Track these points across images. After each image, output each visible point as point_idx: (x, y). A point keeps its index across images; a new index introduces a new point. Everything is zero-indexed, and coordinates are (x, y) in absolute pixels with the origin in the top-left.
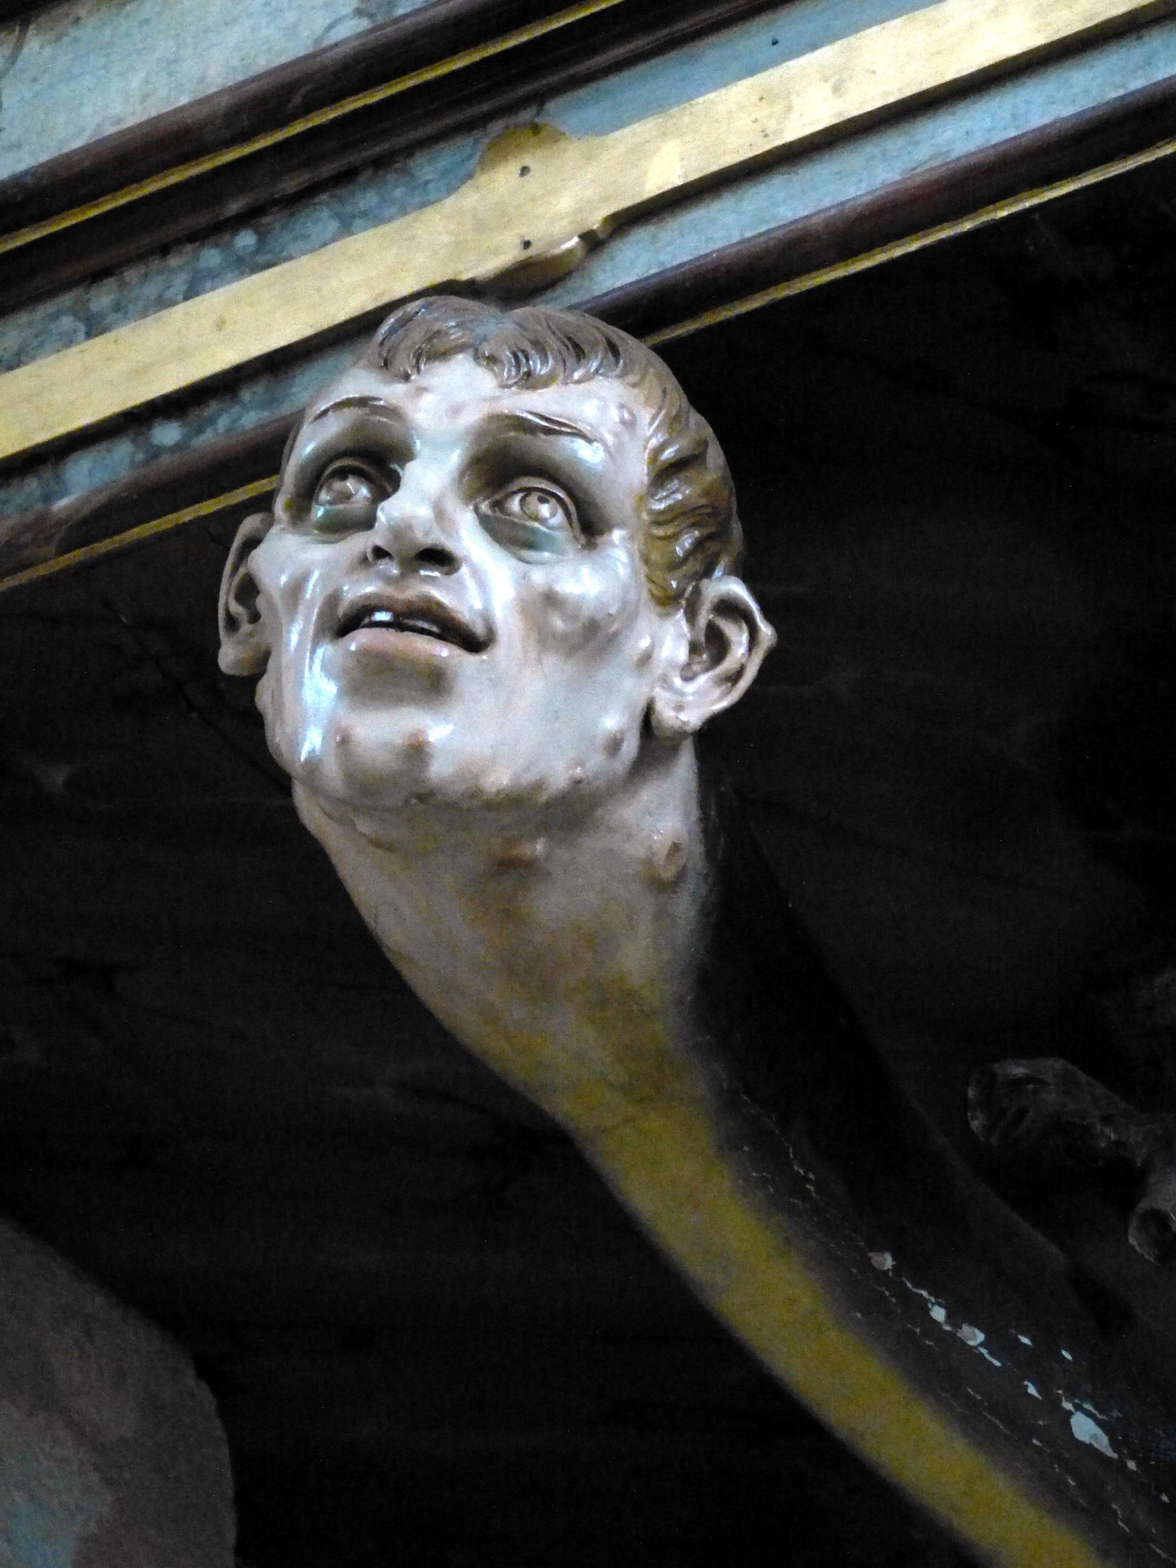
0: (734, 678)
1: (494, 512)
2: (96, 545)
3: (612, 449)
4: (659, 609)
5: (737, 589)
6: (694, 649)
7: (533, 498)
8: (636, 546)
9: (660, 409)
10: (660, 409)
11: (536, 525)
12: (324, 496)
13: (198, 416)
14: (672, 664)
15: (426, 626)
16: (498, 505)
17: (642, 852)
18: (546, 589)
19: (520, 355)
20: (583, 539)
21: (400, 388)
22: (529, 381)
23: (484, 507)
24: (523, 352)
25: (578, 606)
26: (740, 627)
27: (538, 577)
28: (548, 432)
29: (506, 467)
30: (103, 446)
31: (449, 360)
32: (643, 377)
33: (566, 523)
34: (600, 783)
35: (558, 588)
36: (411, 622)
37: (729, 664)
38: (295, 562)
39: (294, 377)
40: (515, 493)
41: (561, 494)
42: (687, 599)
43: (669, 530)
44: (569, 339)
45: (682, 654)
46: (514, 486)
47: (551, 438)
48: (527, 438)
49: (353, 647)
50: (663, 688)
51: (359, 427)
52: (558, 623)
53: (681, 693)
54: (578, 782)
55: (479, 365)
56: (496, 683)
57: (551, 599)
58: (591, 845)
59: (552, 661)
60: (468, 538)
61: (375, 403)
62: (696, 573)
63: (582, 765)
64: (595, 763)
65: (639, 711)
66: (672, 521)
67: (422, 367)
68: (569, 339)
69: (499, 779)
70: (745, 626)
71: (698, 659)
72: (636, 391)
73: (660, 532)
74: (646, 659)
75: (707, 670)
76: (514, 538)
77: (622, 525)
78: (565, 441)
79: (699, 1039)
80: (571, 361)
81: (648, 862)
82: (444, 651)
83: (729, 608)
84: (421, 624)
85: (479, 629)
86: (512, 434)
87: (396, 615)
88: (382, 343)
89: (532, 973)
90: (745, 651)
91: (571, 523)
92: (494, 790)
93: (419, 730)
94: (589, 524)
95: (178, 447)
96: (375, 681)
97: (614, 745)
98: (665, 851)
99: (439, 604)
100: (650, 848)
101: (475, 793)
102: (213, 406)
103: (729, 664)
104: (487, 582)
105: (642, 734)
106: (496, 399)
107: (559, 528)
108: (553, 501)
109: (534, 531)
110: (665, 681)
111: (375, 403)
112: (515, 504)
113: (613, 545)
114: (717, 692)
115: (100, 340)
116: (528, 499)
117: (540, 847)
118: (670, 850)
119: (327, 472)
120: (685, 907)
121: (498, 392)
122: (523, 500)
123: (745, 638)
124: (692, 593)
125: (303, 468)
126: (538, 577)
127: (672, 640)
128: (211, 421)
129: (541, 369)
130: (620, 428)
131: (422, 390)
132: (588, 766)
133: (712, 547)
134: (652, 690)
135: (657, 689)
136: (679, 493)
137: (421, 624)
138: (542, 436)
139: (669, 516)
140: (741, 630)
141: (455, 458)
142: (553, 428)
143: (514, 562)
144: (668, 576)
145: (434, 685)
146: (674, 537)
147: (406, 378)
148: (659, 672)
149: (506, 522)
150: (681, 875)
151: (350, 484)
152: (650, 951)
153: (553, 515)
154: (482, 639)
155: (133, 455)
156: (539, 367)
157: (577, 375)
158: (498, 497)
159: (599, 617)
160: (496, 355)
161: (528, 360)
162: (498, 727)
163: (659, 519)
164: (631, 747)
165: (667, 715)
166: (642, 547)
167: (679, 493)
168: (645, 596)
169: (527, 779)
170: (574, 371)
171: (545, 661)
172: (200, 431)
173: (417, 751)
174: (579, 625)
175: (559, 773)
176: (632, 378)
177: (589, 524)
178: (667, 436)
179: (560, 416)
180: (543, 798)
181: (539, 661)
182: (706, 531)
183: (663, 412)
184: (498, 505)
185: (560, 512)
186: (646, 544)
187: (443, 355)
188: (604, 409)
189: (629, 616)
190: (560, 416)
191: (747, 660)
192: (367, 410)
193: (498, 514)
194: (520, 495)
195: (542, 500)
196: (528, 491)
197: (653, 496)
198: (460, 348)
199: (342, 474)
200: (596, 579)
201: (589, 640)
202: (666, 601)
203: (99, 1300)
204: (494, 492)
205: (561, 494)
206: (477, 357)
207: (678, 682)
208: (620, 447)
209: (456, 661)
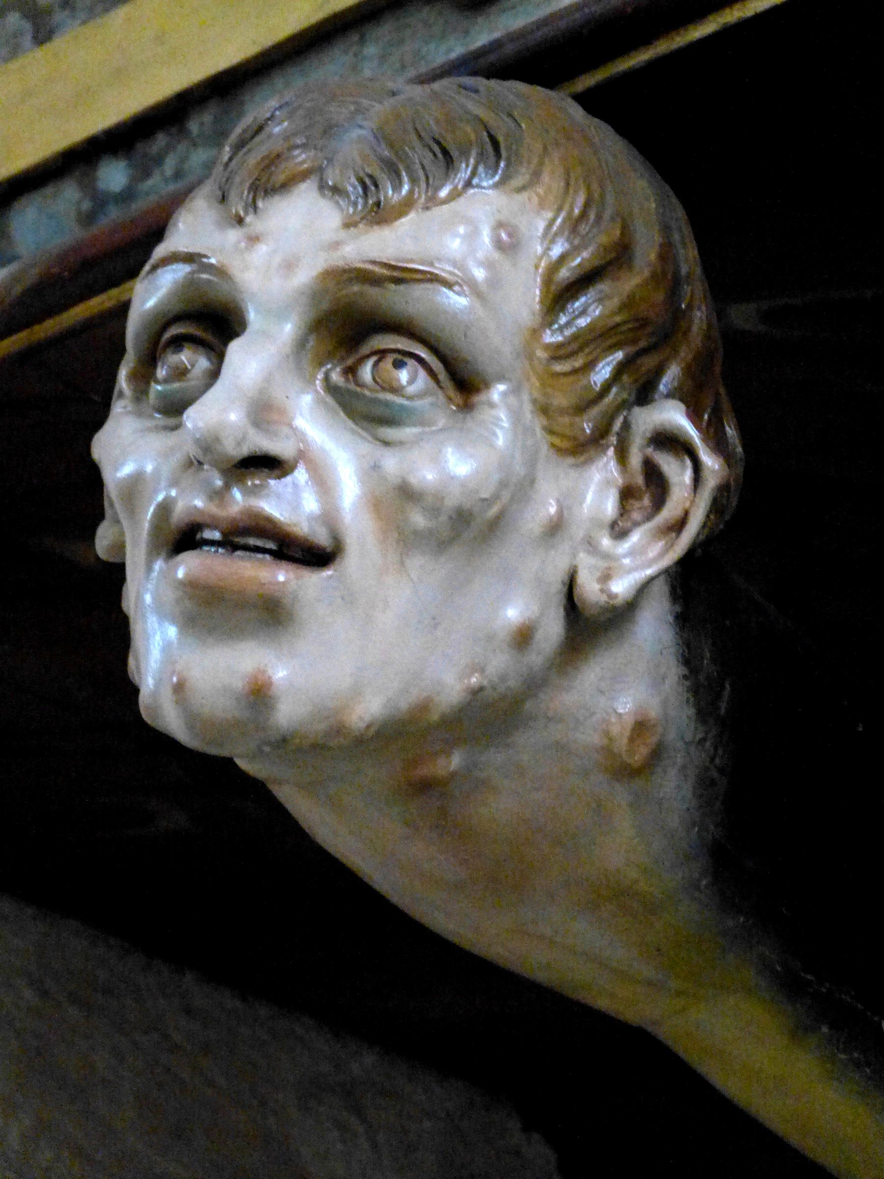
0: (679, 525)
1: (347, 380)
2: (37, 328)
3: (484, 288)
4: (570, 460)
5: (674, 416)
6: (627, 494)
7: (387, 364)
8: (526, 397)
9: (559, 210)
10: (559, 210)
11: (389, 397)
12: (161, 372)
13: (145, 155)
14: (596, 522)
15: (259, 543)
16: (351, 371)
17: (596, 739)
18: (400, 480)
19: (368, 181)
20: (458, 398)
21: (233, 235)
22: (379, 214)
23: (336, 377)
24: (370, 177)
25: (439, 497)
26: (683, 461)
27: (392, 464)
28: (398, 281)
29: (358, 327)
30: (49, 190)
31: (289, 191)
32: (536, 175)
33: (432, 383)
34: (513, 683)
35: (413, 480)
36: (242, 540)
37: (670, 511)
38: (130, 451)
39: (242, 103)
40: (368, 357)
41: (423, 353)
42: (618, 434)
43: (578, 362)
44: (438, 143)
45: (610, 506)
46: (365, 350)
47: (402, 287)
48: (373, 292)
49: (181, 574)
50: (589, 552)
51: (190, 283)
52: (418, 519)
53: (607, 556)
54: (477, 692)
55: (323, 195)
56: (349, 599)
57: (406, 493)
58: (527, 743)
59: (417, 562)
60: (310, 422)
61: (205, 260)
62: (624, 402)
63: (482, 670)
64: (500, 663)
65: (557, 587)
66: (581, 349)
67: (260, 204)
68: (438, 143)
69: (369, 709)
70: (688, 463)
71: (637, 504)
72: (525, 195)
73: (559, 367)
74: (555, 528)
75: (649, 518)
76: (369, 415)
77: (501, 378)
78: (418, 291)
79: (730, 923)
80: (436, 170)
81: (607, 751)
82: (282, 575)
83: (668, 441)
84: (252, 541)
85: (322, 538)
86: (356, 288)
87: (224, 534)
88: (227, 165)
89: (506, 873)
90: (694, 489)
91: (437, 381)
92: (362, 725)
93: (259, 670)
94: (463, 382)
95: (127, 196)
96: (212, 612)
97: (523, 637)
98: (627, 733)
99: (269, 519)
100: (607, 733)
101: (339, 730)
102: (161, 140)
103: (670, 511)
104: (333, 474)
105: (566, 609)
106: (336, 245)
107: (420, 395)
108: (411, 362)
109: (387, 404)
110: (591, 545)
111: (205, 260)
112: (366, 372)
113: (492, 405)
114: (660, 545)
115: (49, 47)
116: (381, 364)
117: (456, 761)
118: (633, 729)
119: (167, 335)
120: (674, 788)
121: (343, 234)
122: (376, 364)
123: (688, 476)
124: (622, 428)
125: (137, 336)
126: (392, 464)
127: (597, 488)
128: (159, 161)
129: (390, 195)
130: (496, 255)
131: (254, 239)
132: (488, 672)
133: (649, 362)
134: (574, 555)
135: (582, 555)
136: (588, 311)
137: (252, 541)
138: (392, 286)
139: (574, 346)
140: (684, 467)
141: (288, 330)
142: (401, 275)
143: (366, 447)
144: (577, 419)
145: (271, 615)
146: (590, 366)
147: (240, 221)
148: (581, 534)
149: (357, 396)
150: (657, 754)
151: (185, 357)
152: (643, 838)
153: (411, 381)
154: (329, 550)
155: (79, 203)
156: (390, 192)
157: (443, 193)
158: (350, 362)
159: (467, 505)
160: (340, 186)
161: (376, 186)
162: (350, 656)
163: (558, 353)
164: (553, 629)
165: (590, 588)
166: (536, 395)
167: (588, 311)
168: (544, 449)
169: (414, 696)
170: (438, 189)
171: (408, 562)
172: (146, 174)
173: (259, 695)
174: (443, 518)
175: (449, 681)
176: (518, 181)
177: (463, 382)
178: (567, 246)
179: (412, 261)
180: (435, 717)
181: (402, 564)
182: (631, 349)
183: (563, 215)
184: (351, 371)
185: (422, 374)
186: (543, 385)
187: (285, 187)
188: (473, 235)
189: (522, 489)
190: (412, 261)
191: (693, 502)
192: (195, 267)
193: (352, 386)
194: (373, 359)
195: (398, 365)
196: (382, 354)
197: (550, 325)
198: (304, 176)
199: (178, 343)
200: (453, 461)
201: (467, 529)
202: (579, 449)
203: (369, 1059)
204: (343, 359)
205: (423, 353)
206: (322, 187)
207: (606, 542)
208: (494, 282)
209: (293, 584)
